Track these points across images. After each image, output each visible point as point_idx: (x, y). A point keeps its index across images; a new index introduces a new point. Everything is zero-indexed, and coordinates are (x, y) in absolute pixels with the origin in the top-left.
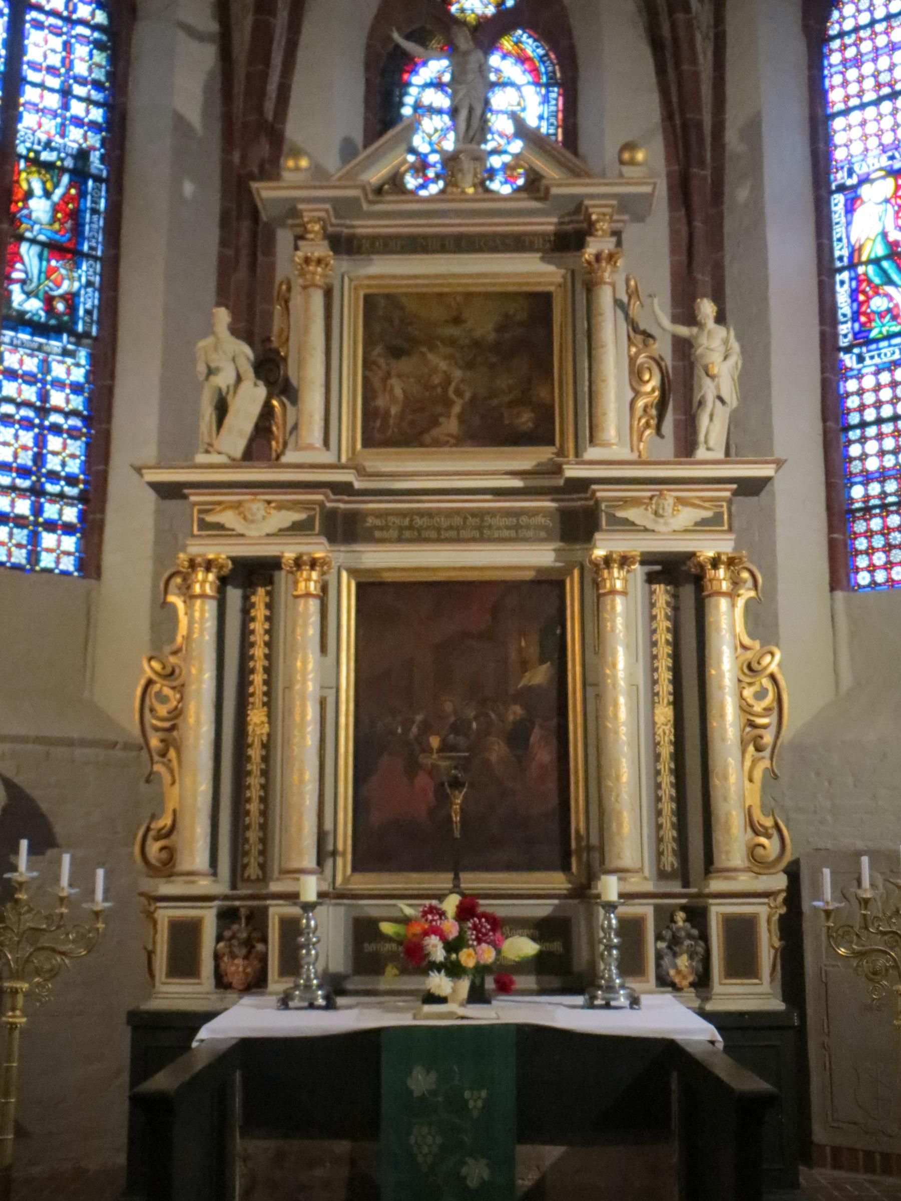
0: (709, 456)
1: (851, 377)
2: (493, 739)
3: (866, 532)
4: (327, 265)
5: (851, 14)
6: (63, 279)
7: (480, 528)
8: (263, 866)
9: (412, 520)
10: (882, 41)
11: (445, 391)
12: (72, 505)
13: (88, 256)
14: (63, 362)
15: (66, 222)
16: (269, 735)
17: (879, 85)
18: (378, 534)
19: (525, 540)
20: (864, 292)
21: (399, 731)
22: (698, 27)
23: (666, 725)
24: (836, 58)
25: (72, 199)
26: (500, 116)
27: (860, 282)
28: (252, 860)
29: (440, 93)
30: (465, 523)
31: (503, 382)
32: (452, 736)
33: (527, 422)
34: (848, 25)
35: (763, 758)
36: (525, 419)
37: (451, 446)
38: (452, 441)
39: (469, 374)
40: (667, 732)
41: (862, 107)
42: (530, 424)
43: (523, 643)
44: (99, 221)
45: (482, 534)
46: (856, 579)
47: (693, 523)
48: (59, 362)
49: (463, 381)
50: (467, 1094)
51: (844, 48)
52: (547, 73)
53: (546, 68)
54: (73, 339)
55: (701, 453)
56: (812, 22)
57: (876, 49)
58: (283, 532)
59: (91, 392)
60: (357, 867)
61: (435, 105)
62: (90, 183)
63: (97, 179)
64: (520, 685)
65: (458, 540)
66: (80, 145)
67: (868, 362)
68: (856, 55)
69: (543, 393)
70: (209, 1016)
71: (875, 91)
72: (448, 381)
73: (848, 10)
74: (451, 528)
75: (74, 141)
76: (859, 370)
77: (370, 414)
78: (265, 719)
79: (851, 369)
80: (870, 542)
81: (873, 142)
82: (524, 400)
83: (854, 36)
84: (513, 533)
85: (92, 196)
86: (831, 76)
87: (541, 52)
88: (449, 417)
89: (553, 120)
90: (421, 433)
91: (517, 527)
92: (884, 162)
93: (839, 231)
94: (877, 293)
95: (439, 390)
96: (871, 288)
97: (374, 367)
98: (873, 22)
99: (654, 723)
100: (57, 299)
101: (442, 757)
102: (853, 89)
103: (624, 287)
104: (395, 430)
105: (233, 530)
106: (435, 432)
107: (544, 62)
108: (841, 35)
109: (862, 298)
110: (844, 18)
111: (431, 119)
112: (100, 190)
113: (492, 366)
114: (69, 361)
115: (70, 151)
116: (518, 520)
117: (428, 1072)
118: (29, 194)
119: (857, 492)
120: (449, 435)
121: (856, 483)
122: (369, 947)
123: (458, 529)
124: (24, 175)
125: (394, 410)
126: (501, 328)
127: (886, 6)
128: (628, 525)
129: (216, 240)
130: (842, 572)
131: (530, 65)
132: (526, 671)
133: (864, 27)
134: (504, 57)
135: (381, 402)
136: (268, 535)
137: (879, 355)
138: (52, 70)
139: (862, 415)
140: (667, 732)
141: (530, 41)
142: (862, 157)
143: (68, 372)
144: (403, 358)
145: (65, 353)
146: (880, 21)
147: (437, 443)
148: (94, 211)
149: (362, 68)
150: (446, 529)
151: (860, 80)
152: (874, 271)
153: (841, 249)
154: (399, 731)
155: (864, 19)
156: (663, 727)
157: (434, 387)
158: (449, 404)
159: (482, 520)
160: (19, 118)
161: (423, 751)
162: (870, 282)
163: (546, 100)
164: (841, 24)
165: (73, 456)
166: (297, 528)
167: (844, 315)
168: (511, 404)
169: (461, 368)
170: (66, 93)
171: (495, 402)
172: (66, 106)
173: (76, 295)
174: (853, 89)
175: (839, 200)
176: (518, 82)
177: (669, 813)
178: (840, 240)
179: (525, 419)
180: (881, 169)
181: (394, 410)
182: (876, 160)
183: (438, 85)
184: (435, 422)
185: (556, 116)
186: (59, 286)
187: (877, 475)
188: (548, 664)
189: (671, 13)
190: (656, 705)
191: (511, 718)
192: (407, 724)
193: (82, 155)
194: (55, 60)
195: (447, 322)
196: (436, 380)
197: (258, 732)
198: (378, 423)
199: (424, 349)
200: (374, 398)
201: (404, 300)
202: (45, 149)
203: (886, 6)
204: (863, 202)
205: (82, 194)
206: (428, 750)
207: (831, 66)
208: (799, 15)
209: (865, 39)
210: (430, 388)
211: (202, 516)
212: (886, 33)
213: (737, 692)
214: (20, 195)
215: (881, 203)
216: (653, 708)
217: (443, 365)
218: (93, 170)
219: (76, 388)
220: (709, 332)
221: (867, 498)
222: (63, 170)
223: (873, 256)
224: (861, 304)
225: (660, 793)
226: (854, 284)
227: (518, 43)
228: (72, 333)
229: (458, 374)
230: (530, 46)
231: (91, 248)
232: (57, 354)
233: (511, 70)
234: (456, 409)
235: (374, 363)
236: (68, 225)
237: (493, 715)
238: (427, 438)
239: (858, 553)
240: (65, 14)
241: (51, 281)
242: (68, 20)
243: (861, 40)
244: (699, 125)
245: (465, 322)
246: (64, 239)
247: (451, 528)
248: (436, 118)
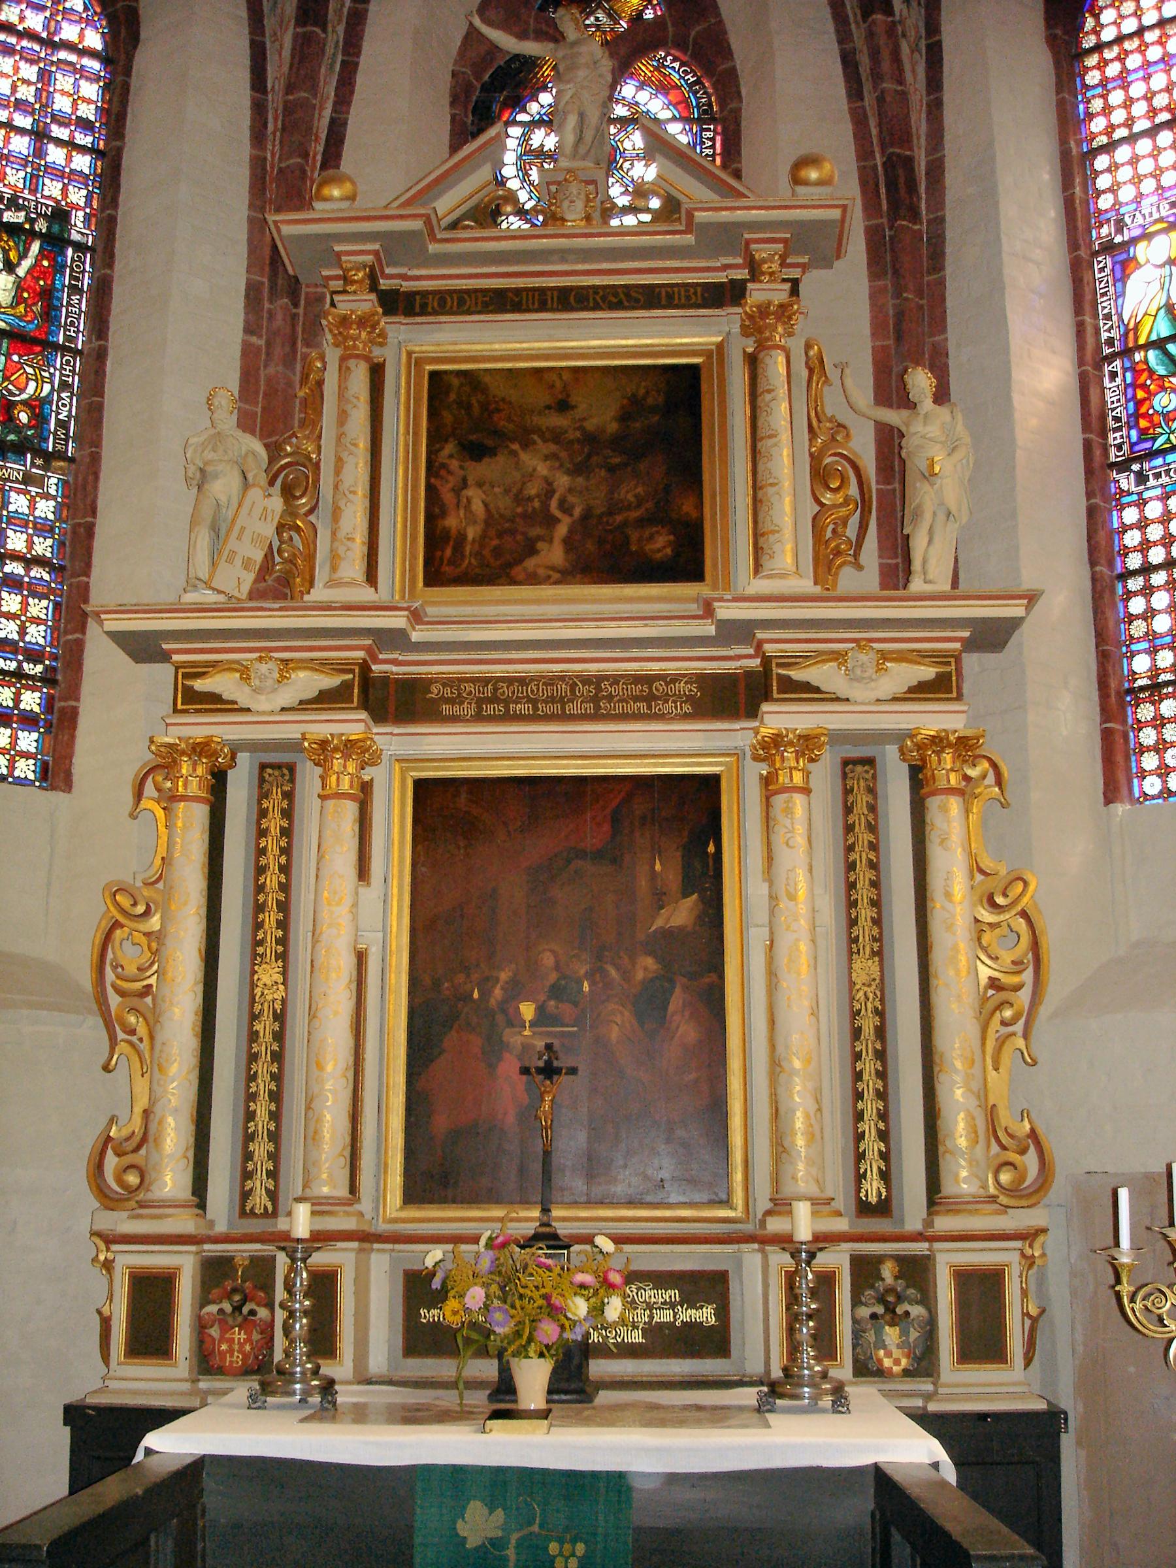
0: (928, 588)
1: (1129, 504)
2: (611, 1006)
3: (1154, 719)
4: (374, 327)
5: (1112, 20)
6: (28, 379)
7: (595, 700)
8: (273, 1195)
9: (495, 689)
10: (1154, 53)
11: (545, 506)
12: (33, 689)
13: (64, 349)
14: (26, 492)
15: (35, 304)
16: (284, 1001)
17: (1153, 112)
18: (446, 709)
19: (660, 717)
20: (1144, 387)
21: (476, 995)
22: (904, 36)
23: (870, 985)
24: (1093, 78)
25: (44, 274)
27: (1137, 373)
28: (258, 1184)
30: (573, 691)
31: (630, 491)
32: (552, 1003)
33: (664, 547)
34: (1108, 35)
35: (1014, 1034)
36: (660, 544)
37: (555, 583)
38: (556, 576)
39: (580, 480)
40: (871, 996)
41: (1132, 139)
42: (669, 551)
43: (658, 867)
44: (80, 300)
45: (598, 708)
46: (1140, 786)
47: (906, 689)
48: (19, 491)
49: (570, 490)
50: (553, 1548)
51: (1103, 64)
53: (697, 99)
54: (39, 462)
55: (917, 585)
56: (1059, 32)
57: (1147, 64)
58: (305, 705)
59: (63, 533)
60: (411, 1196)
62: (70, 252)
63: (79, 247)
64: (653, 928)
65: (563, 717)
66: (57, 202)
67: (1152, 482)
68: (1121, 72)
69: (688, 507)
70: (161, 1417)
71: (1149, 118)
72: (549, 492)
73: (1108, 16)
74: (552, 700)
75: (50, 197)
76: (1140, 494)
77: (436, 539)
78: (280, 979)
79: (1129, 493)
80: (1159, 733)
81: (1148, 185)
82: (659, 517)
83: (1116, 49)
84: (642, 706)
85: (72, 270)
86: (1089, 102)
88: (551, 541)
90: (510, 565)
91: (650, 698)
93: (1105, 305)
94: (1162, 388)
95: (537, 504)
96: (1153, 380)
97: (443, 473)
98: (1140, 32)
99: (852, 984)
100: (19, 407)
101: (541, 1033)
102: (1118, 116)
103: (804, 359)
104: (473, 561)
105: (235, 703)
106: (530, 563)
107: (695, 93)
108: (1099, 47)
109: (1140, 394)
110: (1102, 26)
112: (84, 263)
113: (612, 469)
114: (34, 490)
116: (650, 688)
117: (492, 1510)
119: (1141, 664)
120: (553, 568)
121: (1139, 652)
122: (428, 1315)
123: (562, 701)
125: (471, 533)
126: (625, 417)
127: (1159, 9)
128: (807, 691)
129: (241, 325)
130: (1121, 777)
131: (676, 96)
132: (662, 907)
133: (1130, 36)
135: (452, 522)
136: (283, 709)
137: (1167, 472)
139: (1145, 557)
140: (871, 996)
142: (1134, 206)
143: (32, 506)
144: (486, 460)
145: (28, 479)
146: (1151, 28)
147: (533, 579)
148: (75, 290)
149: (446, 101)
150: (546, 702)
151: (1128, 103)
152: (1157, 356)
153: (1109, 331)
154: (476, 995)
155: (1130, 26)
156: (866, 989)
157: (530, 499)
158: (552, 522)
159: (599, 689)
161: (511, 1024)
162: (1151, 372)
164: (1098, 34)
165: (37, 621)
166: (326, 699)
167: (1117, 419)
168: (641, 523)
169: (569, 472)
170: (40, 136)
171: (619, 518)
173: (47, 400)
174: (1118, 116)
177: (874, 1117)
178: (1108, 317)
179: (660, 544)
180: (1161, 220)
181: (471, 533)
182: (1154, 209)
184: (531, 550)
186: (22, 390)
187: (1168, 639)
188: (695, 896)
189: (866, 15)
190: (855, 956)
191: (640, 975)
192: (486, 984)
193: (60, 215)
195: (549, 407)
196: (532, 490)
197: (269, 997)
198: (448, 552)
199: (515, 447)
200: (444, 514)
201: (487, 379)
202: (8, 208)
203: (1159, 9)
204: (1139, 266)
205: (58, 268)
206: (516, 1022)
207: (1088, 88)
208: (1042, 23)
209: (1132, 52)
210: (519, 499)
211: (189, 683)
212: (1161, 42)
213: (975, 936)
215: (1162, 266)
216: (850, 960)
217: (543, 469)
218: (75, 236)
219: (43, 528)
220: (926, 415)
221: (1155, 671)
222: (33, 234)
223: (1154, 337)
224: (1139, 403)
225: (860, 1086)
226: (1129, 376)
228: (39, 452)
229: (563, 481)
230: (675, 71)
231: (68, 338)
232: (17, 481)
234: (562, 530)
235: (444, 466)
236: (37, 308)
237: (613, 972)
238: (517, 572)
239: (1142, 750)
240: (44, 35)
241: (11, 383)
243: (1127, 53)
244: (909, 162)
245: (573, 407)
246: (31, 326)
247: (552, 700)
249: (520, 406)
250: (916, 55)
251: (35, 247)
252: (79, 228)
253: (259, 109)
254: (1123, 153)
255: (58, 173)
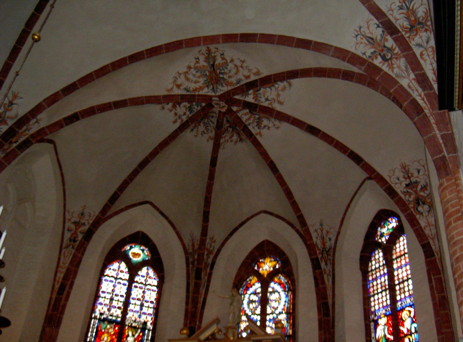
22: (325, 273)
26: (273, 302)
29: (255, 296)
52: (288, 288)
61: (254, 300)
63: (149, 330)
87: (286, 281)
89: (289, 302)
92: (384, 311)
93: (373, 335)
111: (252, 304)
115: (141, 323)
118: (128, 336)
124: (127, 331)
134: (275, 283)
138: (138, 299)
141: (283, 278)
160: (127, 314)
163: (287, 296)
172: (141, 309)
175: (372, 324)
176: (279, 291)
183: (255, 293)
185: (290, 301)
193: (145, 323)
194: (140, 297)
205: (144, 335)
214: (125, 336)
227: (279, 278)
230: (283, 279)
233: (278, 287)
242: (146, 285)
248: (254, 304)
249: (442, 178)
250: (329, 277)
251: (139, 331)
252: (149, 326)
253: (187, 297)
254: (376, 297)
255: (145, 314)
